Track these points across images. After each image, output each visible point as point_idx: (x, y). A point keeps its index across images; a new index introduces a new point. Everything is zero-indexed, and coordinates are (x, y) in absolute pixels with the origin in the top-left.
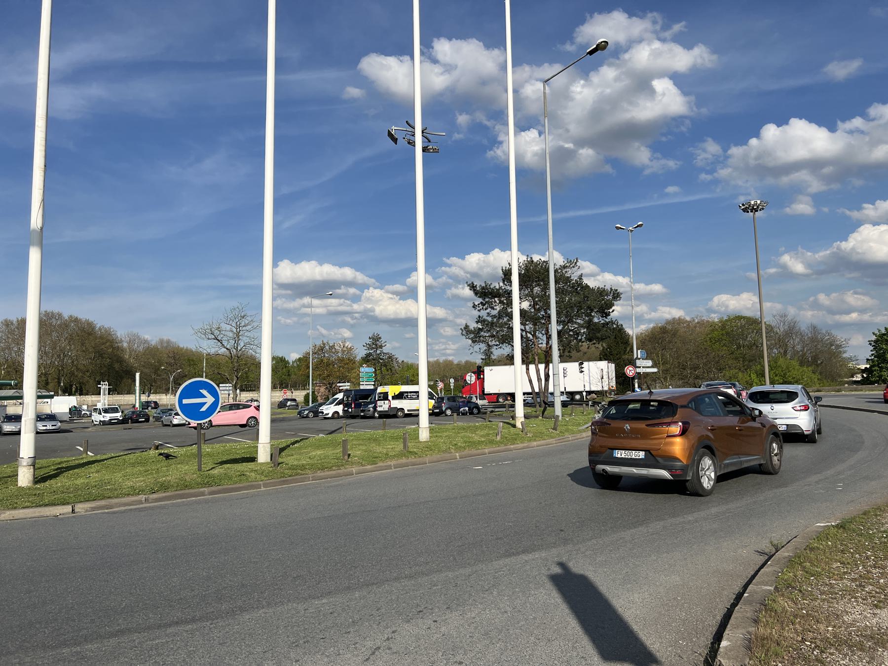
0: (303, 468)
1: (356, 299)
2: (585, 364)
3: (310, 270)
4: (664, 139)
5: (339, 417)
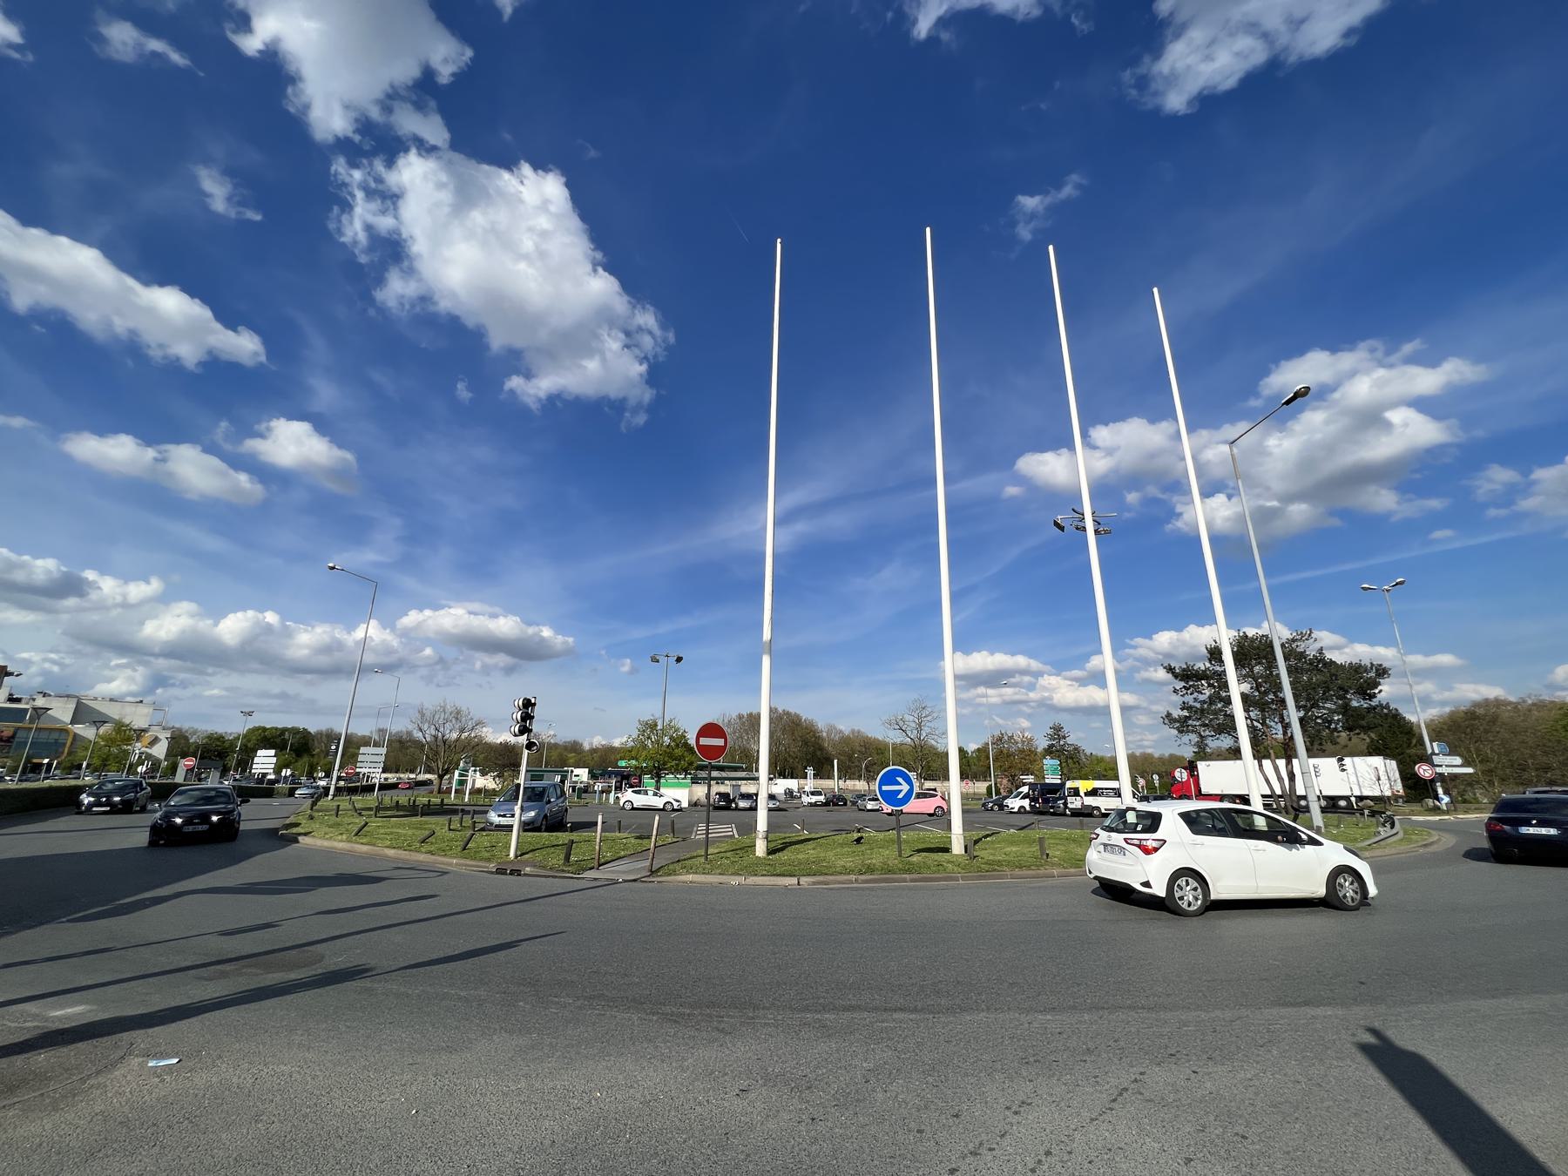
0: (999, 863)
1: (1031, 687)
2: (1347, 760)
3: (983, 661)
4: (1418, 476)
5: (1026, 812)
